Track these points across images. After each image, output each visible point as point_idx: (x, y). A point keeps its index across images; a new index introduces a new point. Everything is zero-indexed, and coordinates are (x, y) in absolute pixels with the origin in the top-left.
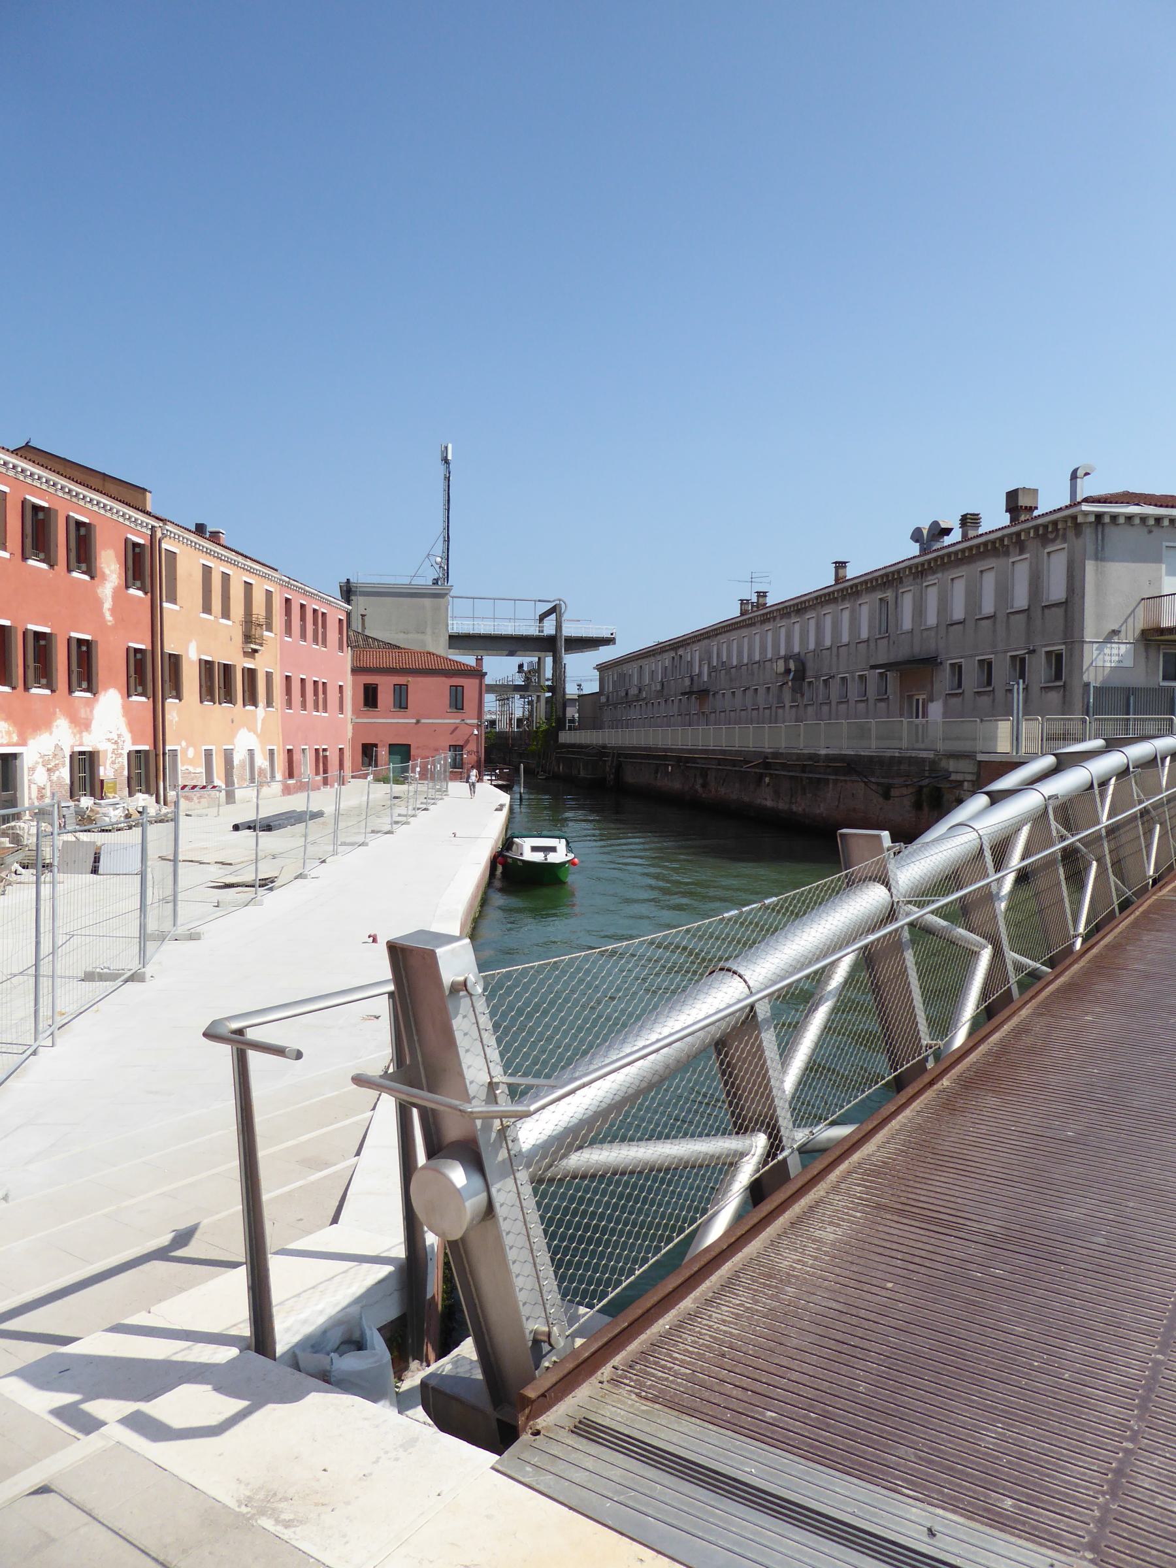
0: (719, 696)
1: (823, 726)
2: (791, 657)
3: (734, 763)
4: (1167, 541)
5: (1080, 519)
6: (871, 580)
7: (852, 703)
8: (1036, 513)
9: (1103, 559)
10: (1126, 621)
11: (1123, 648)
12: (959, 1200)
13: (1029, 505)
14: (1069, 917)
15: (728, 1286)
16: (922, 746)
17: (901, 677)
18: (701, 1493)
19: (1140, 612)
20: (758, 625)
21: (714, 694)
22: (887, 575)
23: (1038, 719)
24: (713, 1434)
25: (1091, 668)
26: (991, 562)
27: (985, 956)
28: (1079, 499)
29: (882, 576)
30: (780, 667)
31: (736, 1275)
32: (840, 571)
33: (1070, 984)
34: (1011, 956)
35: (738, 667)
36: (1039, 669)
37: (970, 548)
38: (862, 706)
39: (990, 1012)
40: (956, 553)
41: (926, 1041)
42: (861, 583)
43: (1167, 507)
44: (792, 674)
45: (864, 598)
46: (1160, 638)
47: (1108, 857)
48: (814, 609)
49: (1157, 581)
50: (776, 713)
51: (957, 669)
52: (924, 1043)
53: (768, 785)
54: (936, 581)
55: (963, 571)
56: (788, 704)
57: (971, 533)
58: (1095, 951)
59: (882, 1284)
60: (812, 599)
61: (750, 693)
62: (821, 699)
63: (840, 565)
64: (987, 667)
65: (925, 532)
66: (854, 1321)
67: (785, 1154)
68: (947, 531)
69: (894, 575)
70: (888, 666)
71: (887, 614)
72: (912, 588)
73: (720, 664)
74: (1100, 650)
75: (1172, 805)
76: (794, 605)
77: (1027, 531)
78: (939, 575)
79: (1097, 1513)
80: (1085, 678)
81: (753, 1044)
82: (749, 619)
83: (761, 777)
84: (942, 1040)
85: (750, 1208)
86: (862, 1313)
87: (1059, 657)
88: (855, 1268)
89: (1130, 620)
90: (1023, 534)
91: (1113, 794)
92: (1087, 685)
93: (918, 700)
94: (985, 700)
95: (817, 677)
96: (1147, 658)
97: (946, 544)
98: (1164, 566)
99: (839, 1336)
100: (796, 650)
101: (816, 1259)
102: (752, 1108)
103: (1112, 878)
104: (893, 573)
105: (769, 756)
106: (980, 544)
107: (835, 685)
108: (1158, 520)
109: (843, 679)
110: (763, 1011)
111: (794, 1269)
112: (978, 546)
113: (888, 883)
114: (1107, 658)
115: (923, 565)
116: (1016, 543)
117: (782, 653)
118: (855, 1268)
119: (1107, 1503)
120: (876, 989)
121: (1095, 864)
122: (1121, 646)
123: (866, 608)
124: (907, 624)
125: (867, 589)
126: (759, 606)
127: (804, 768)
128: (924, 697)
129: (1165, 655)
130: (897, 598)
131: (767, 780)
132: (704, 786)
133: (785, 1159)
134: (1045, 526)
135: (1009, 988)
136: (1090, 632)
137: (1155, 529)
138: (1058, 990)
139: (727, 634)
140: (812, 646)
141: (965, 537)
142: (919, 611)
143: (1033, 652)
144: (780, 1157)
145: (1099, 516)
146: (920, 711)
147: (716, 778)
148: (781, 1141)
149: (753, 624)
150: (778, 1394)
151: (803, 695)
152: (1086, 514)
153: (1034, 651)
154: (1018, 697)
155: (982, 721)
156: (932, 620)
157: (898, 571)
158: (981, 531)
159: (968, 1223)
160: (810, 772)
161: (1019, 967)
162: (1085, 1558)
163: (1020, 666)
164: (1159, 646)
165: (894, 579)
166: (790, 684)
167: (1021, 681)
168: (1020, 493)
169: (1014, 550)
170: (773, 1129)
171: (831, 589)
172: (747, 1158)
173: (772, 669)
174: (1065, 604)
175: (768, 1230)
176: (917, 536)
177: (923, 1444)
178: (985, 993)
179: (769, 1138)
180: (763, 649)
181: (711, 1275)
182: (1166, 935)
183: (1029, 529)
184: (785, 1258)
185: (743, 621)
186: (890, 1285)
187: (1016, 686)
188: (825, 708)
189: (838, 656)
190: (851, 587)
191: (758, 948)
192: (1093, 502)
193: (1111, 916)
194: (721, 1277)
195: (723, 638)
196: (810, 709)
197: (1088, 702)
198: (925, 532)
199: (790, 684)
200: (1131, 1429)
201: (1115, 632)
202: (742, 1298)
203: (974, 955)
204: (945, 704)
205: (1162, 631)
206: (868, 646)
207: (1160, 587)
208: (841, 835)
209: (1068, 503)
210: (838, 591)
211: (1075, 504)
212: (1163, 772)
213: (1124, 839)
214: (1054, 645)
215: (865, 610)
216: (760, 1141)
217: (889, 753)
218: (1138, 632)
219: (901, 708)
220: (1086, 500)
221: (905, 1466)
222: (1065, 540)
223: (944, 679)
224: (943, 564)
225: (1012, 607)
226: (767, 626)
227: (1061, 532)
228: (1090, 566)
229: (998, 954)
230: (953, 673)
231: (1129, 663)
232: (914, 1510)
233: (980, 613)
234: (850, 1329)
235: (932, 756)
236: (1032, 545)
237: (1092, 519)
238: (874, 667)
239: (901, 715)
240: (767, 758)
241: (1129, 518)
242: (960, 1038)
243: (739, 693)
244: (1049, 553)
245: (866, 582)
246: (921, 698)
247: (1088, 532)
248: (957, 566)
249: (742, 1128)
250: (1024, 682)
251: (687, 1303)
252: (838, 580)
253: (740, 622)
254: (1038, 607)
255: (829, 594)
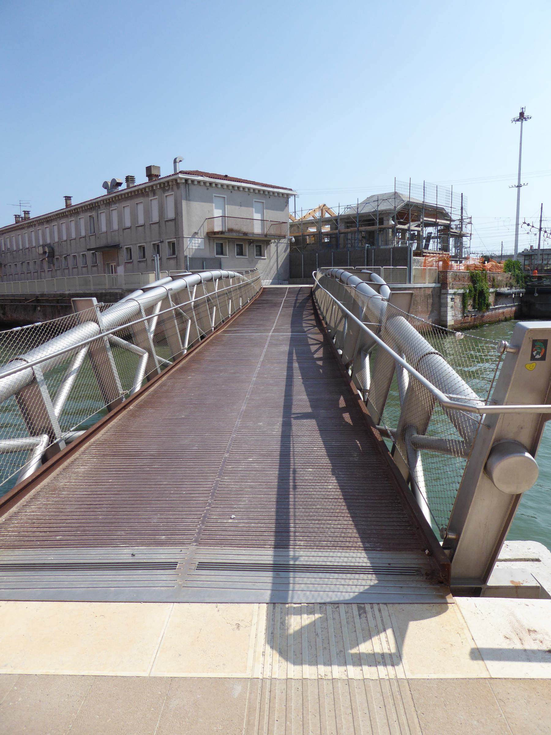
0: (8, 267)
1: (66, 279)
2: (46, 245)
3: (20, 301)
4: (215, 194)
5: (179, 181)
6: (84, 206)
7: (80, 268)
8: (160, 177)
9: (189, 200)
10: (200, 228)
11: (200, 240)
12: (139, 446)
13: (156, 174)
14: (180, 341)
15: (34, 498)
16: (116, 288)
17: (103, 254)
18: (27, 573)
19: (206, 224)
20: (26, 229)
21: (5, 266)
22: (92, 204)
23: (166, 272)
24: (31, 552)
25: (187, 249)
26: (141, 199)
27: (146, 356)
28: (178, 172)
29: (89, 205)
30: (41, 250)
31: (38, 493)
32: (68, 202)
33: (182, 367)
34: (157, 357)
35: (17, 251)
36: (165, 250)
37: (131, 192)
38: (84, 269)
39: (147, 378)
40: (124, 194)
41: (121, 391)
42: (79, 208)
43: (214, 178)
44: (47, 254)
45: (82, 215)
46: (214, 236)
47: (195, 317)
48: (56, 221)
49: (211, 211)
50: (41, 275)
51: (129, 250)
52: (121, 392)
53: (40, 311)
54: (116, 208)
55: (128, 203)
56: (46, 270)
57: (131, 185)
58: (192, 355)
59: (107, 481)
60: (55, 215)
61: (25, 265)
62: (63, 266)
63: (68, 198)
64: (142, 249)
65: (109, 184)
66: (95, 496)
67: (57, 440)
68: (120, 184)
69: (95, 204)
70: (96, 249)
71: (93, 223)
72: (105, 211)
73: (6, 249)
74: (191, 241)
75: (220, 298)
76: (45, 218)
77: (156, 185)
78: (117, 205)
79: (197, 531)
80: (185, 254)
81: (35, 391)
82: (20, 225)
83: (35, 307)
84: (128, 390)
85: (42, 464)
86: (99, 493)
87: (174, 244)
88: (94, 478)
89: (202, 228)
90: (154, 186)
91: (196, 292)
92: (186, 257)
93: (112, 266)
94: (143, 265)
95: (61, 256)
96: (209, 245)
97: (120, 190)
98: (214, 205)
99: (89, 503)
100: (48, 241)
101: (76, 479)
102: (39, 424)
103: (197, 327)
104: (95, 203)
105: (39, 296)
106: (136, 190)
107: (70, 259)
108: (211, 184)
109: (74, 256)
110: (39, 377)
111: (66, 485)
112: (134, 191)
113: (97, 321)
114: (194, 245)
115: (109, 199)
116: (152, 191)
117: (41, 243)
118: (94, 478)
119: (201, 527)
120: (95, 367)
121: (190, 321)
122: (199, 239)
123: (83, 220)
124: (104, 229)
125: (82, 210)
126: (25, 219)
127: (58, 301)
128: (115, 264)
129: (216, 243)
130: (98, 215)
131: (39, 308)
132: (4, 314)
133: (57, 443)
134: (164, 184)
135: (157, 369)
136: (186, 232)
137: (210, 188)
138: (177, 370)
139: (10, 233)
140: (56, 240)
141: (128, 186)
142: (109, 222)
143: (162, 242)
144: (55, 442)
145: (186, 180)
146: (113, 270)
147: (10, 309)
148: (54, 435)
149: (23, 228)
150: (62, 529)
151: (54, 265)
152: (181, 179)
153: (163, 241)
154: (157, 263)
155: (142, 274)
156: (115, 227)
157: (97, 202)
158: (135, 184)
159: (143, 453)
160: (61, 303)
161: (160, 362)
162: (193, 545)
163: (157, 248)
164: (214, 240)
165: (96, 206)
166: (47, 259)
167: (158, 255)
168: (152, 168)
169: (151, 194)
170: (52, 434)
171: (64, 211)
172: (38, 446)
173: (36, 252)
174: (175, 220)
175: (52, 474)
176: (105, 185)
177: (128, 529)
178: (146, 372)
179: (50, 437)
180: (30, 241)
181: (25, 496)
182: (219, 347)
183: (157, 184)
184: (62, 482)
185: (17, 226)
186: (110, 481)
187: (156, 258)
188: (66, 271)
189: (71, 245)
190: (75, 210)
191: (35, 351)
192: (183, 173)
193: (197, 341)
194: (30, 496)
195: (7, 236)
196: (58, 271)
197: (187, 264)
198: (109, 184)
199: (47, 259)
200: (208, 503)
201: (196, 233)
202: (43, 500)
203: (141, 357)
204: (125, 267)
205: (215, 233)
206: (86, 239)
207: (213, 214)
208: (73, 301)
209: (173, 173)
210: (68, 211)
211: (176, 174)
212: (216, 285)
213: (201, 310)
214: (171, 238)
215: (82, 222)
216: (45, 438)
217: (100, 291)
218: (205, 234)
219: (104, 270)
220: (181, 172)
221: (121, 537)
222: (173, 190)
223: (123, 255)
224: (119, 200)
225: (152, 221)
226: (31, 229)
227: (171, 187)
228: (184, 203)
229: (151, 356)
230: (127, 252)
231: (202, 247)
232: (125, 550)
233: (138, 224)
234: (93, 499)
235: (120, 292)
236: (159, 192)
237: (184, 181)
238: (89, 250)
239: (105, 273)
240: (38, 297)
241: (199, 182)
242: (138, 387)
243: (19, 265)
244: (166, 196)
245: (82, 207)
246: (113, 264)
247: (182, 187)
248: (125, 201)
249: (34, 433)
250: (159, 256)
251: (14, 509)
252: (67, 206)
253: (15, 227)
254: (163, 222)
255: (63, 213)
